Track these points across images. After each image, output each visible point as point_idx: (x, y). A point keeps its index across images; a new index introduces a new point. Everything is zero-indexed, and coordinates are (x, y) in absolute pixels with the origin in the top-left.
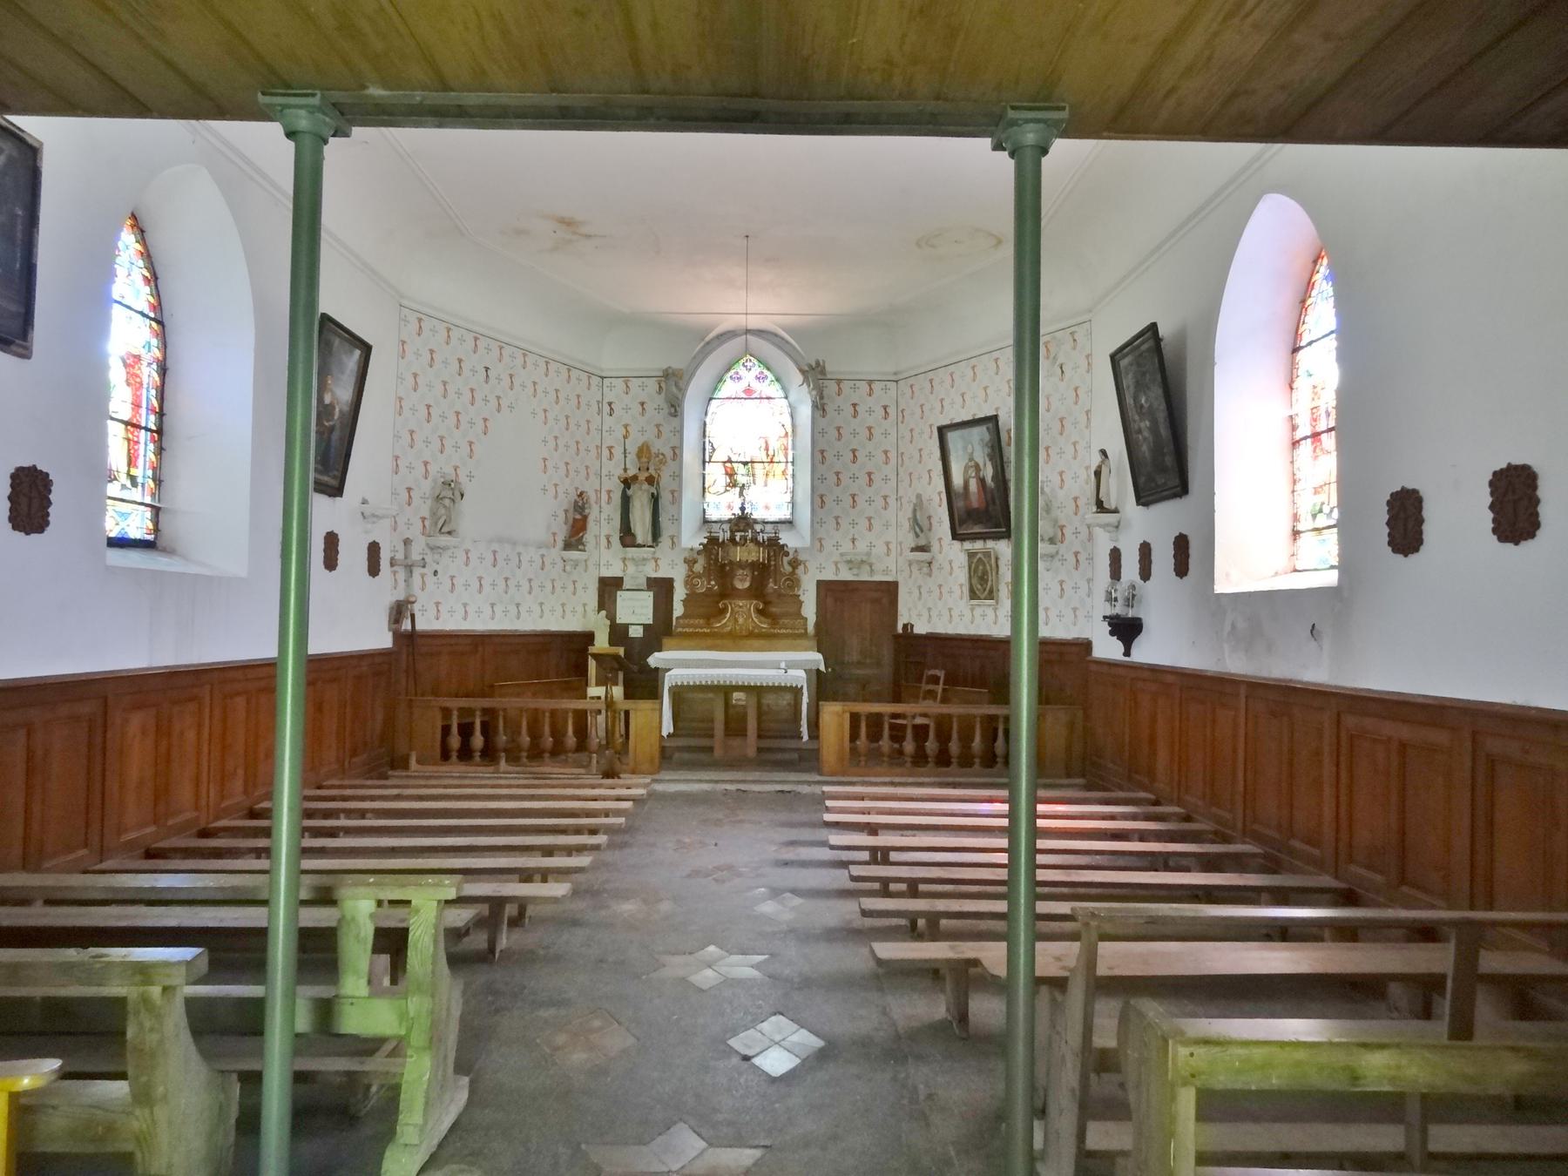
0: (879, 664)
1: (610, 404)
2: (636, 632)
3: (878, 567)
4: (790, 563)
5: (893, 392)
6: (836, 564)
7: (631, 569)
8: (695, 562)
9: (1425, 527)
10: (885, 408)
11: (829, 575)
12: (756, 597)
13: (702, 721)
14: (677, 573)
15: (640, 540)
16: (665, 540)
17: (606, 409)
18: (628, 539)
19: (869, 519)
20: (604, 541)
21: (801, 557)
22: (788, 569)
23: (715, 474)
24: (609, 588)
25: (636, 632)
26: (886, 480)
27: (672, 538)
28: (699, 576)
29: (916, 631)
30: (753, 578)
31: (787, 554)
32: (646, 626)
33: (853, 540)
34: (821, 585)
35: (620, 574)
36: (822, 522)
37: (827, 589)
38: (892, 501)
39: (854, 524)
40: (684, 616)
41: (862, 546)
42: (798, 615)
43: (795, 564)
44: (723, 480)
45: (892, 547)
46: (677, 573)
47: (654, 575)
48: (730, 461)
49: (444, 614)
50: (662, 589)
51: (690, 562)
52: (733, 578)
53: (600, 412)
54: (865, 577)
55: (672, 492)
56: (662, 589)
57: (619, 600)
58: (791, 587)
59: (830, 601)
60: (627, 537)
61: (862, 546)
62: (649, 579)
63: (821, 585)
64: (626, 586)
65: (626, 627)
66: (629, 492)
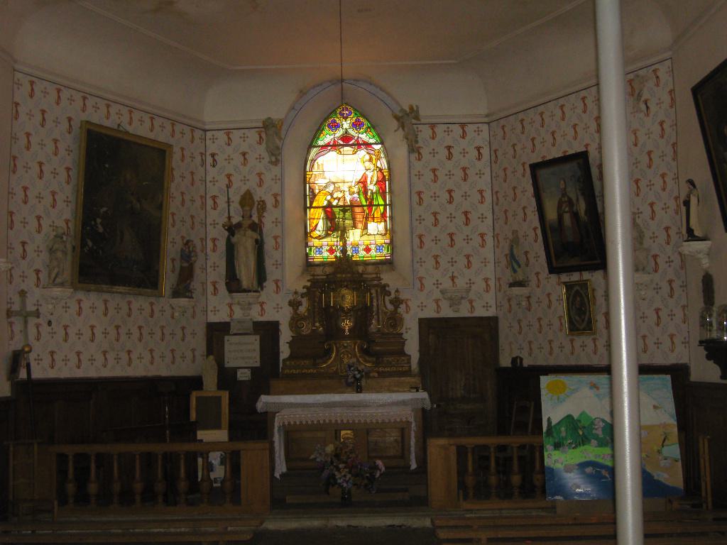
1: (213, 155)
4: (391, 302)
5: (485, 134)
6: (437, 301)
8: (300, 304)
11: (430, 313)
15: (245, 284)
16: (270, 285)
17: (209, 160)
19: (468, 257)
20: (210, 289)
22: (390, 307)
25: (244, 375)
26: (482, 218)
27: (276, 282)
28: (304, 318)
32: (254, 370)
33: (453, 278)
35: (228, 320)
40: (291, 357)
42: (402, 353)
43: (397, 302)
45: (492, 283)
47: (261, 319)
50: (268, 331)
51: (294, 304)
55: (276, 238)
58: (394, 326)
60: (233, 283)
61: (461, 283)
64: (233, 330)
65: (235, 370)
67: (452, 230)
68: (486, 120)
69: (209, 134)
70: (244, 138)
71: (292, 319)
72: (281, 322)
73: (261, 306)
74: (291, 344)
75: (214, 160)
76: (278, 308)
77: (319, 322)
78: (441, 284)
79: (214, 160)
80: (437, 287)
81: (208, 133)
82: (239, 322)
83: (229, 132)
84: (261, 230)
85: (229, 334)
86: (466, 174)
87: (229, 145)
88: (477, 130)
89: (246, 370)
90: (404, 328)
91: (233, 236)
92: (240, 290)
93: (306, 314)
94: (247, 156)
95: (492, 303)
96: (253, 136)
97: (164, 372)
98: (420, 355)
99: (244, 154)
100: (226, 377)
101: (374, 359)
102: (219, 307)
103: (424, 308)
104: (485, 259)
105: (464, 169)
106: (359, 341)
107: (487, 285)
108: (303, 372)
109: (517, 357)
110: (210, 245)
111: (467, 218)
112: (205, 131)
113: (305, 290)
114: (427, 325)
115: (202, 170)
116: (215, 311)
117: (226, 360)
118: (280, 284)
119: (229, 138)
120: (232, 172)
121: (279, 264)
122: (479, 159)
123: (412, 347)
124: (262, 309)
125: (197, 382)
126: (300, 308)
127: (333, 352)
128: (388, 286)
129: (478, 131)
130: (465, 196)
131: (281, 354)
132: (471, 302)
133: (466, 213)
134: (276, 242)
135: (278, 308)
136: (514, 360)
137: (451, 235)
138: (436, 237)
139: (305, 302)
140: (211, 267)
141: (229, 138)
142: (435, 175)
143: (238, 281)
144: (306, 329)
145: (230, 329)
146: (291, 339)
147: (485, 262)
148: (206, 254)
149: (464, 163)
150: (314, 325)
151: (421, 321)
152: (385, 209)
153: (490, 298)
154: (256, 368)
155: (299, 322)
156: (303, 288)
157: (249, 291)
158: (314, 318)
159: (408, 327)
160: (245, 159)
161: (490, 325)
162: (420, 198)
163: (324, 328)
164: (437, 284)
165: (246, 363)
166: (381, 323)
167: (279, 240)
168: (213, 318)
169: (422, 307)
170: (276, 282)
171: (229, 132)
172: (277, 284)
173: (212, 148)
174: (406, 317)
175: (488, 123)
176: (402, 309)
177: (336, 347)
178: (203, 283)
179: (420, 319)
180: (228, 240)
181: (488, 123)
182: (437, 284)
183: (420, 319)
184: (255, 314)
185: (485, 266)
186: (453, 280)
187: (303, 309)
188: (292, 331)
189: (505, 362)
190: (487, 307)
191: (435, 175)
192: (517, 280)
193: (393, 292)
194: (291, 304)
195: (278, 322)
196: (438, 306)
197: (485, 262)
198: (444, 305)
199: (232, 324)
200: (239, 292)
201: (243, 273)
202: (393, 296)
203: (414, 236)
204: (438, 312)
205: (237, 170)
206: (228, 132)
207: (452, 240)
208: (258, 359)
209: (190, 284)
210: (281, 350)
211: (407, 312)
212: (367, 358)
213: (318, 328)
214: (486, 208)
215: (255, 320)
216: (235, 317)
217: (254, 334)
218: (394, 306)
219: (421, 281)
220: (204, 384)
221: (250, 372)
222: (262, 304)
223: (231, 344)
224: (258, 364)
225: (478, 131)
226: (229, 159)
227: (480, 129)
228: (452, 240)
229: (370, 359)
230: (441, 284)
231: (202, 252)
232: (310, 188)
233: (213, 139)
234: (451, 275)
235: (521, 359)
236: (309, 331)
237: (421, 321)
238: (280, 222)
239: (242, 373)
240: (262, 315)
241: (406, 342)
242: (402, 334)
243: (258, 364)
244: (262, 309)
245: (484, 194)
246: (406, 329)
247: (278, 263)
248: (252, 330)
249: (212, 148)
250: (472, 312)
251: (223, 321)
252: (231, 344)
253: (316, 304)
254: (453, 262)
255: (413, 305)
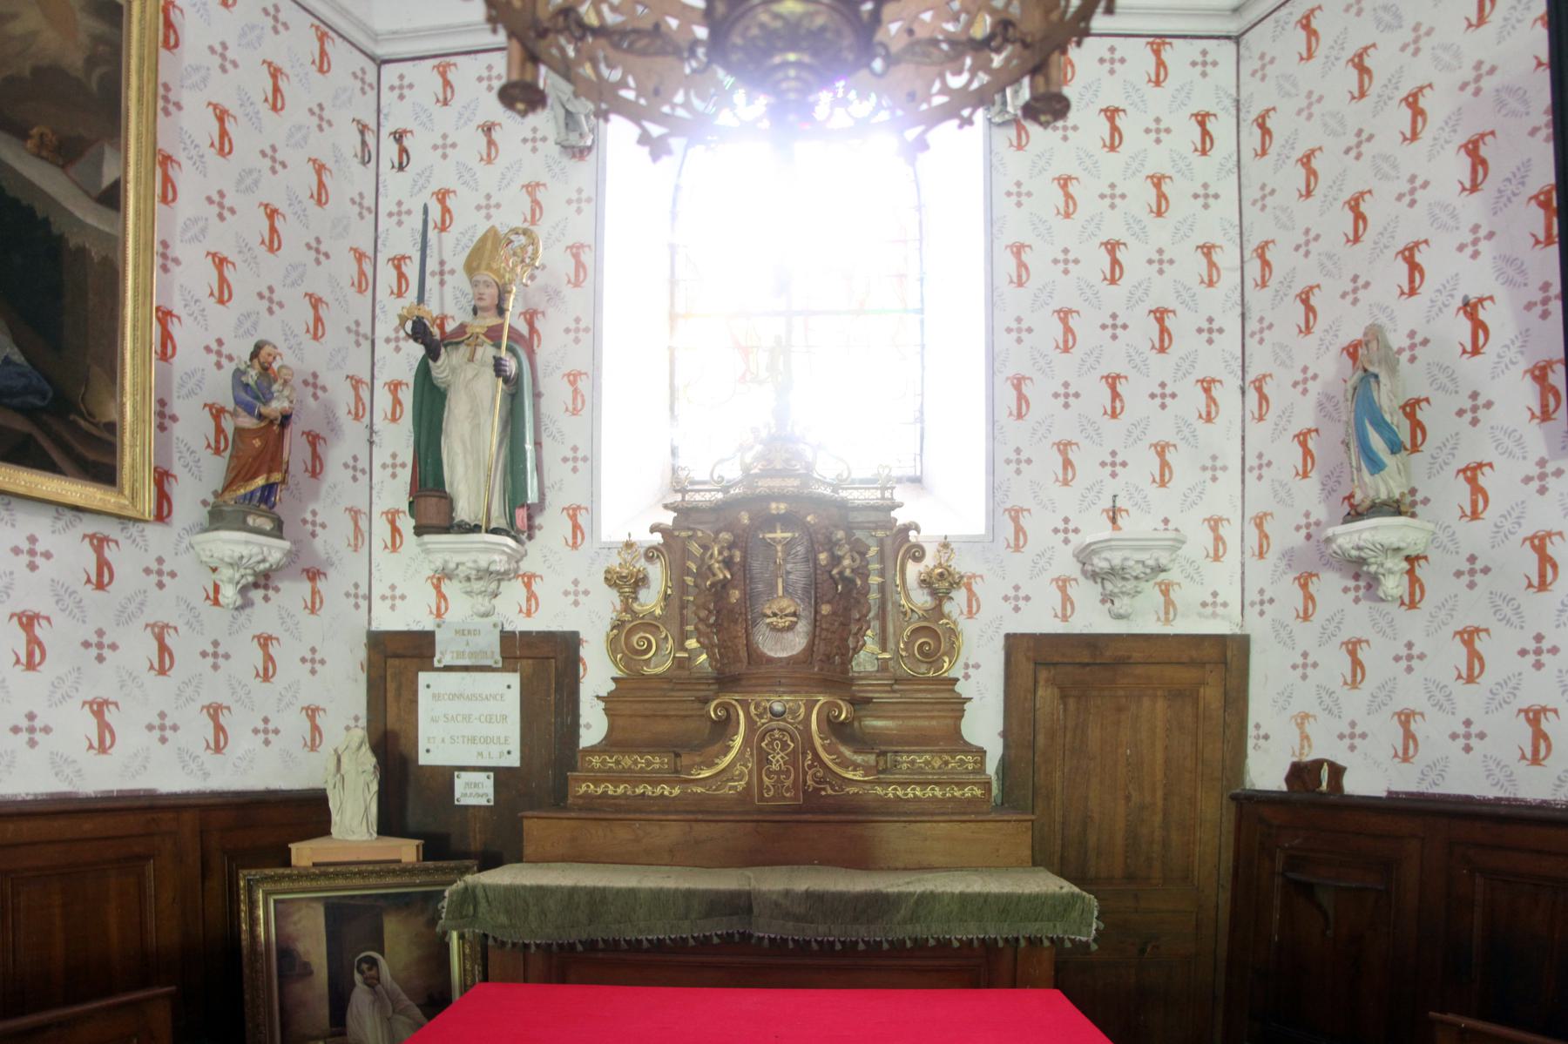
0: (44, 398)
1: (399, 137)
2: (474, 791)
4: (925, 583)
5: (1224, 74)
6: (1063, 584)
7: (461, 607)
8: (640, 581)
9: (1000, 728)
10: (1202, 119)
11: (1041, 620)
14: (590, 618)
15: (464, 511)
16: (553, 526)
17: (389, 150)
18: (430, 504)
19: (1161, 450)
20: (381, 529)
21: (961, 565)
22: (921, 599)
24: (398, 659)
25: (474, 791)
26: (1210, 331)
27: (573, 512)
29: (1357, 784)
31: (917, 553)
32: (502, 776)
33: (1114, 515)
34: (1015, 645)
35: (427, 624)
36: (1020, 461)
38: (1228, 395)
39: (1114, 464)
40: (610, 744)
42: (954, 741)
43: (941, 584)
45: (1230, 533)
46: (590, 618)
49: (242, 741)
50: (545, 663)
51: (627, 583)
52: (750, 627)
53: (366, 156)
54: (1147, 623)
55: (573, 378)
56: (545, 663)
58: (931, 657)
60: (430, 503)
61: (1136, 525)
62: (507, 638)
63: (1015, 645)
64: (443, 656)
65: (446, 775)
68: (1232, 27)
71: (618, 625)
73: (528, 585)
74: (611, 703)
75: (403, 151)
76: (576, 593)
77: (699, 634)
78: (1076, 531)
79: (403, 151)
80: (1066, 541)
81: (386, 69)
84: (531, 354)
86: (1161, 196)
88: (1199, 59)
89: (482, 776)
91: (435, 359)
92: (450, 526)
93: (658, 612)
94: (495, 135)
95: (1231, 595)
98: (1006, 746)
100: (405, 787)
101: (871, 759)
102: (403, 584)
104: (1214, 458)
105: (1157, 181)
106: (822, 699)
107: (1218, 539)
108: (639, 791)
109: (1318, 764)
113: (657, 538)
114: (1031, 657)
115: (362, 179)
118: (582, 519)
119: (447, 83)
124: (531, 596)
125: (308, 812)
126: (643, 594)
128: (917, 529)
129: (1204, 64)
130: (1160, 261)
131: (582, 731)
133: (1160, 315)
136: (1302, 773)
139: (657, 573)
140: (384, 466)
141: (447, 83)
142: (1114, 129)
143: (449, 502)
145: (433, 656)
146: (612, 686)
148: (371, 427)
149: (1158, 161)
153: (1224, 579)
155: (635, 639)
157: (476, 529)
158: (683, 622)
160: (491, 143)
161: (1225, 658)
163: (711, 657)
164: (1066, 530)
165: (480, 754)
166: (891, 645)
167: (583, 384)
168: (389, 620)
169: (1017, 599)
170: (573, 512)
172: (573, 518)
175: (1236, 39)
176: (956, 606)
177: (747, 714)
178: (355, 513)
179: (1008, 636)
181: (1236, 39)
182: (1066, 530)
183: (1008, 636)
185: (1214, 479)
186: (1114, 520)
187: (650, 600)
189: (1266, 772)
192: (1383, 496)
194: (614, 580)
195: (575, 635)
196: (1066, 599)
197: (1214, 468)
198: (1086, 594)
200: (447, 530)
202: (929, 561)
204: (1065, 618)
207: (1115, 395)
208: (515, 744)
210: (582, 721)
211: (971, 615)
212: (847, 752)
213: (693, 654)
214: (1220, 302)
215: (508, 628)
217: (504, 669)
218: (934, 593)
219: (1015, 520)
221: (491, 783)
222: (529, 579)
223: (436, 697)
224: (514, 761)
225: (1204, 64)
226: (445, 147)
227: (1209, 59)
228: (1115, 395)
230: (1076, 531)
234: (1109, 505)
235: (1337, 772)
236: (669, 663)
239: (467, 784)
244: (531, 596)
245: (1217, 257)
246: (967, 666)
251: (415, 628)
252: (436, 697)
253: (689, 580)
254: (1114, 464)
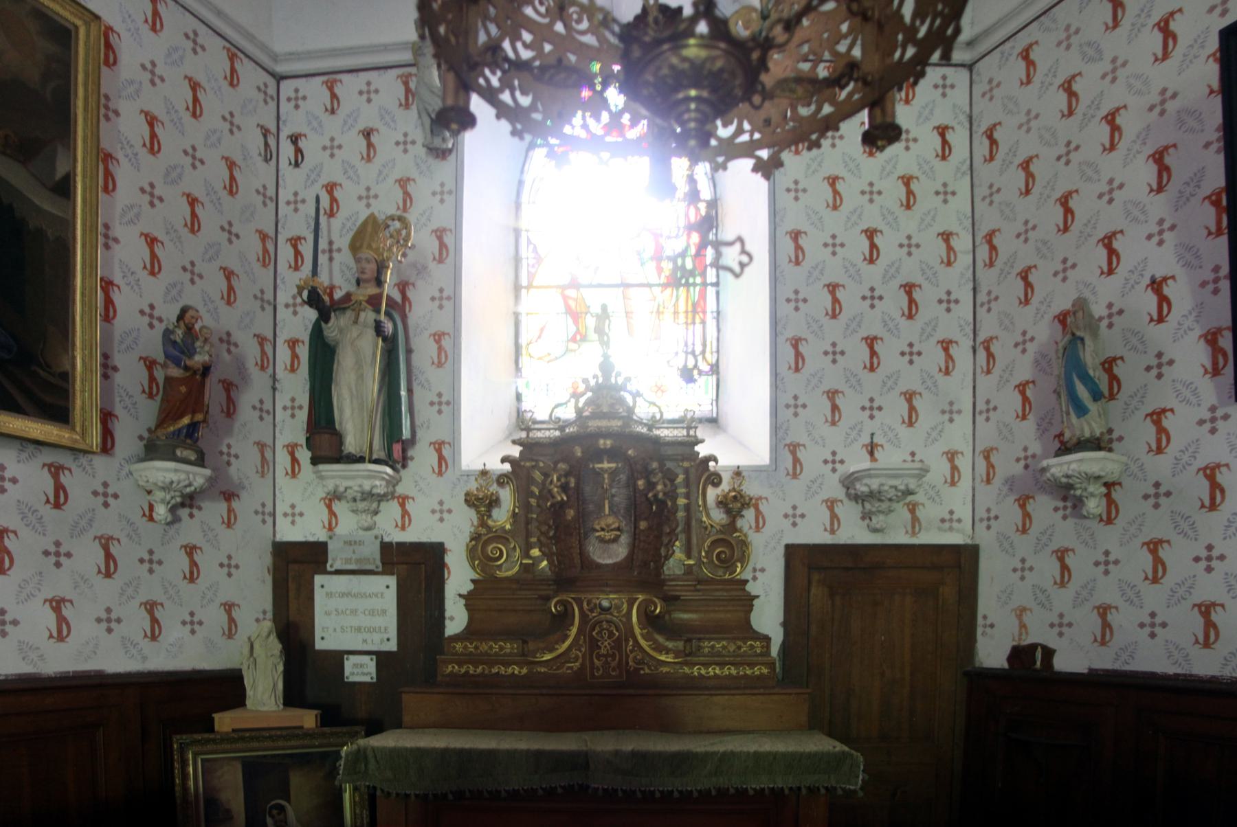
1: (295, 139)
2: (360, 671)
3: (929, 512)
6: (831, 504)
7: (348, 523)
8: (494, 502)
11: (814, 533)
12: (644, 585)
13: (1059, 395)
15: (351, 444)
16: (422, 457)
17: (287, 150)
19: (909, 397)
20: (283, 459)
22: (718, 516)
23: (543, 312)
24: (297, 565)
25: (360, 671)
26: (948, 302)
27: (438, 446)
28: (501, 536)
29: (1065, 662)
30: (635, 535)
31: (715, 479)
32: (382, 658)
33: (872, 449)
35: (321, 536)
37: (804, 562)
38: (962, 353)
39: (872, 409)
40: (470, 633)
41: (890, 458)
42: (745, 630)
43: (735, 504)
44: (563, 326)
45: (964, 463)
46: (453, 532)
47: (398, 537)
48: (575, 285)
50: (416, 567)
51: (482, 503)
54: (899, 537)
57: (390, 622)
58: (728, 564)
59: (817, 592)
60: (324, 441)
61: (890, 458)
62: (386, 548)
64: (336, 559)
65: (337, 658)
66: (331, 330)
67: (876, 330)
69: (287, 87)
70: (368, 93)
71: (476, 537)
72: (447, 546)
73: (402, 505)
74: (470, 600)
76: (442, 512)
79: (298, 151)
80: (834, 470)
81: (284, 84)
82: (349, 543)
83: (335, 81)
84: (404, 318)
85: (325, 572)
87: (333, 112)
89: (366, 659)
90: (750, 568)
91: (327, 321)
92: (340, 457)
93: (508, 527)
94: (374, 139)
95: (964, 512)
96: (389, 86)
97: (116, 659)
99: (367, 134)
102: (301, 505)
103: (798, 520)
106: (641, 597)
107: (954, 469)
108: (495, 670)
110: (283, 354)
111: (912, 301)
112: (279, 78)
114: (804, 562)
116: (294, 515)
117: (318, 634)
119: (334, 96)
120: (338, 177)
121: (449, 404)
122: (944, 158)
123: (768, 617)
124: (405, 513)
125: (226, 687)
126: (495, 513)
127: (572, 624)
128: (716, 460)
130: (909, 245)
131: (447, 622)
132: (913, 509)
133: (909, 288)
134: (440, 349)
135: (442, 512)
136: (1021, 655)
137: (871, 341)
138: (945, 185)
139: (506, 496)
140: (285, 408)
141: (334, 96)
142: (836, 193)
143: (338, 437)
144: (509, 568)
147: (951, 412)
150: (527, 555)
151: (792, 551)
152: (703, 295)
153: (959, 501)
154: (388, 654)
156: (503, 460)
157: (361, 460)
158: (528, 535)
159: (758, 567)
160: (370, 145)
161: (960, 563)
162: (798, 248)
163: (550, 563)
164: (834, 461)
165: (365, 641)
166: (695, 553)
167: (446, 343)
168: (290, 533)
169: (795, 517)
171: (335, 81)
172: (439, 451)
173: (294, 122)
174: (757, 541)
177: (581, 609)
178: (261, 446)
179: (788, 547)
180: (317, 334)
182: (834, 461)
183: (788, 547)
184: (389, 526)
186: (871, 453)
187: (502, 517)
188: (474, 568)
189: (992, 653)
190: (948, 521)
191: (836, 193)
193: (726, 477)
194: (471, 501)
199: (330, 547)
200: (337, 460)
201: (347, 412)
202: (725, 486)
203: (781, 339)
204: (833, 532)
205: (351, 172)
206: (331, 78)
207: (873, 353)
209: (161, 423)
210: (447, 614)
211: (758, 529)
212: (661, 639)
213: (537, 561)
214: (956, 279)
215: (386, 539)
216: (339, 530)
219: (794, 453)
220: (249, 692)
223: (330, 595)
224: (392, 646)
228: (873, 353)
229: (670, 645)
230: (842, 462)
231: (263, 368)
232: (529, 242)
233: (297, 100)
234: (868, 441)
235: (1049, 653)
236: (517, 568)
237: (792, 551)
238: (449, 298)
239: (355, 665)
240: (403, 528)
241: (755, 602)
242: (746, 581)
243: (392, 646)
244: (405, 513)
246: (755, 570)
247: (444, 399)
248: (379, 563)
249: (294, 122)
250: (914, 534)
251: (311, 539)
252: (330, 595)
253: (533, 501)
254: (872, 409)
255: (773, 511)
